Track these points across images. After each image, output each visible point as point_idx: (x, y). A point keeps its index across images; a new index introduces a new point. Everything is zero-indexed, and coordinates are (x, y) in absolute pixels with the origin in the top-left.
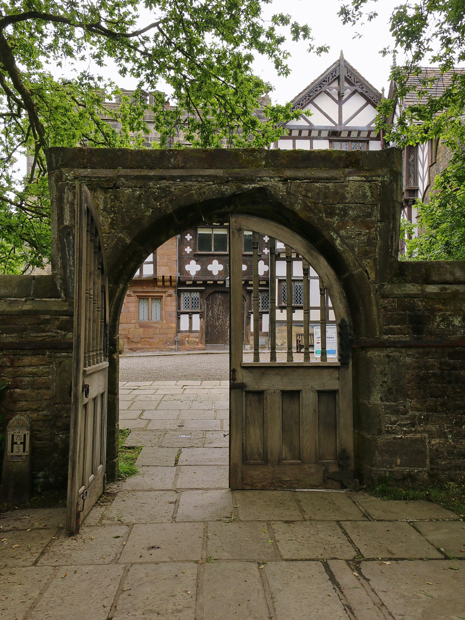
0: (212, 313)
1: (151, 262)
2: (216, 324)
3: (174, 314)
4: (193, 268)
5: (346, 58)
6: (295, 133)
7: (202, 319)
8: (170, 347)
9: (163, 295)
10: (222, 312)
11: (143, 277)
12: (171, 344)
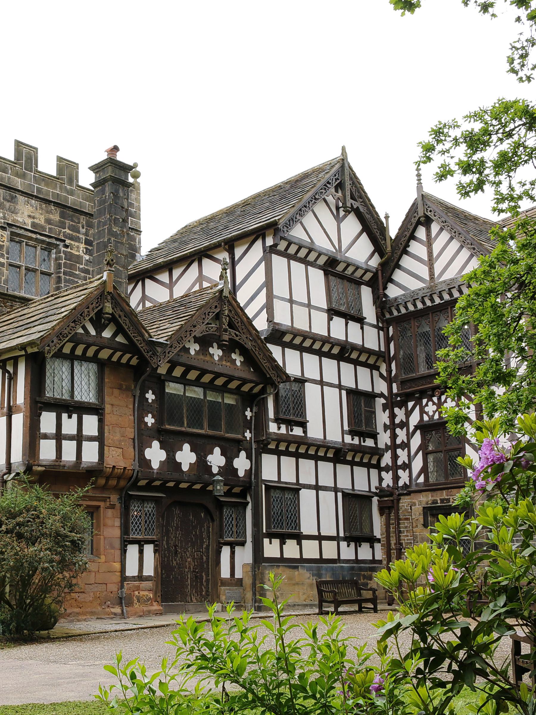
0: (168, 543)
1: (95, 437)
2: (173, 563)
3: (117, 544)
4: (156, 454)
5: (353, 161)
6: (292, 250)
7: (157, 554)
8: (113, 610)
9: (102, 504)
10: (181, 541)
11: (82, 466)
12: (113, 605)
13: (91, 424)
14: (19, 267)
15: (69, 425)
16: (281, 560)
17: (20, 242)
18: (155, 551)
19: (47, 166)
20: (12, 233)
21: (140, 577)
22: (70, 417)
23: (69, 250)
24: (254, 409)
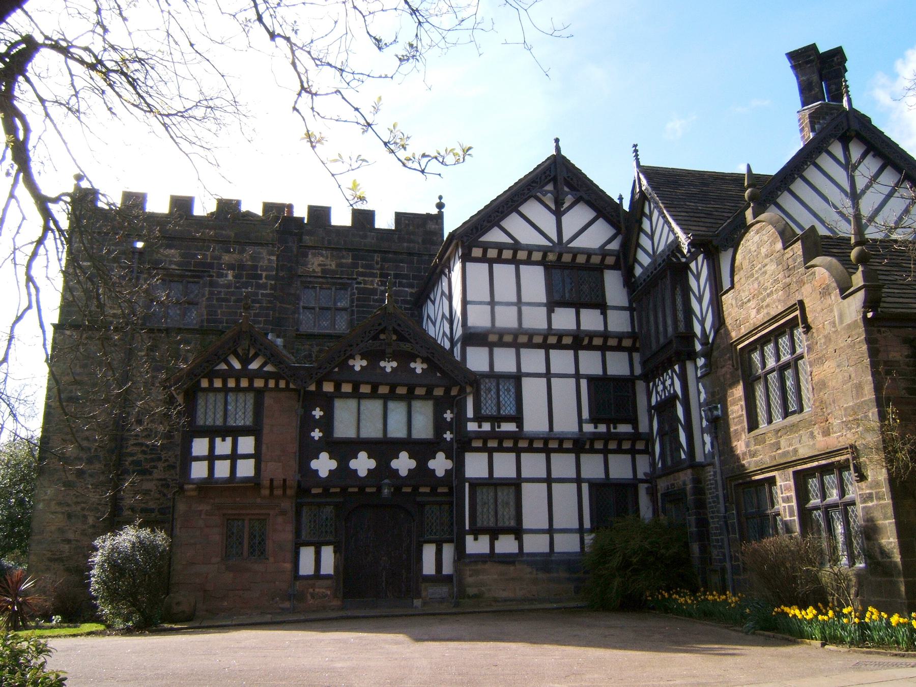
9: (272, 512)
13: (247, 444)
14: (313, 308)
15: (223, 447)
16: (491, 557)
17: (314, 288)
18: (335, 552)
19: (341, 218)
20: (302, 282)
21: (317, 575)
22: (224, 440)
23: (362, 286)
24: (455, 411)
